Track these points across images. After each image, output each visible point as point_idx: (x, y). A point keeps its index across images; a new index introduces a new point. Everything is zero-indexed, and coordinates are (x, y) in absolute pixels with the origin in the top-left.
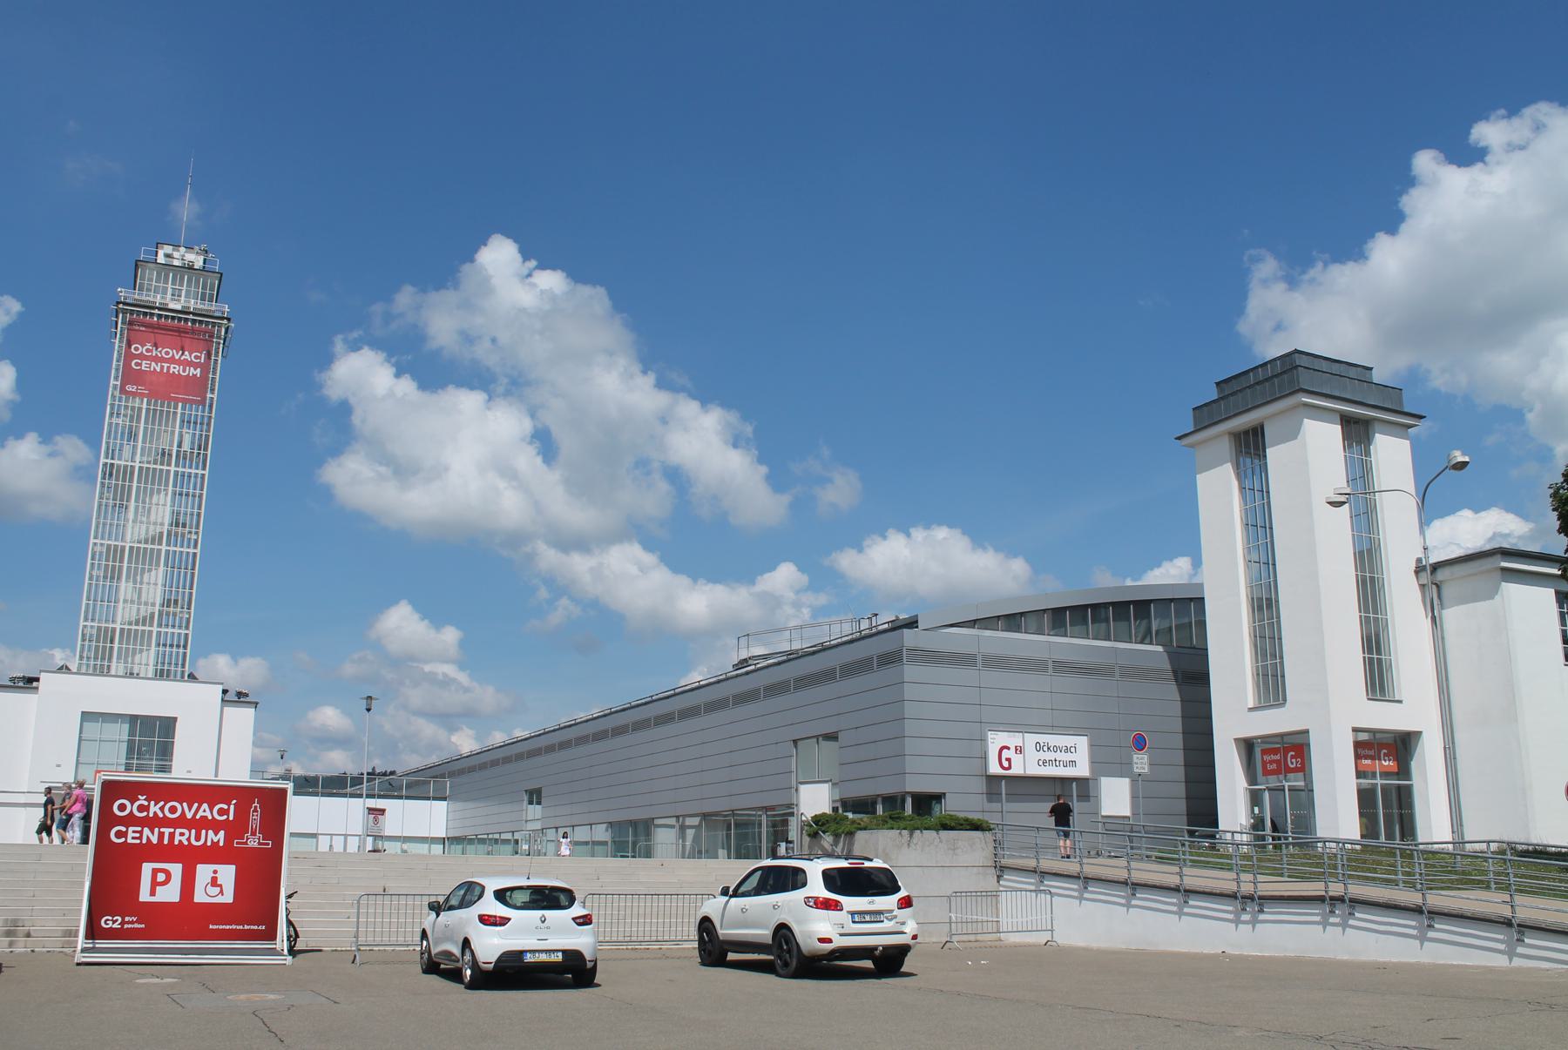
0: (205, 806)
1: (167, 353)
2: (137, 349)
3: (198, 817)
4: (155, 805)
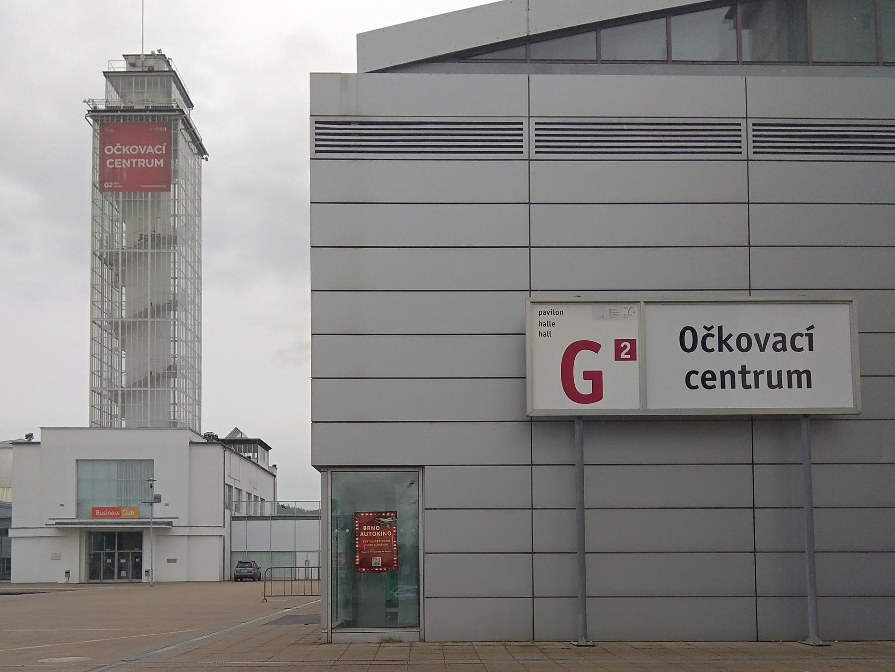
0: (150, 147)
1: (134, 150)
3: (147, 153)
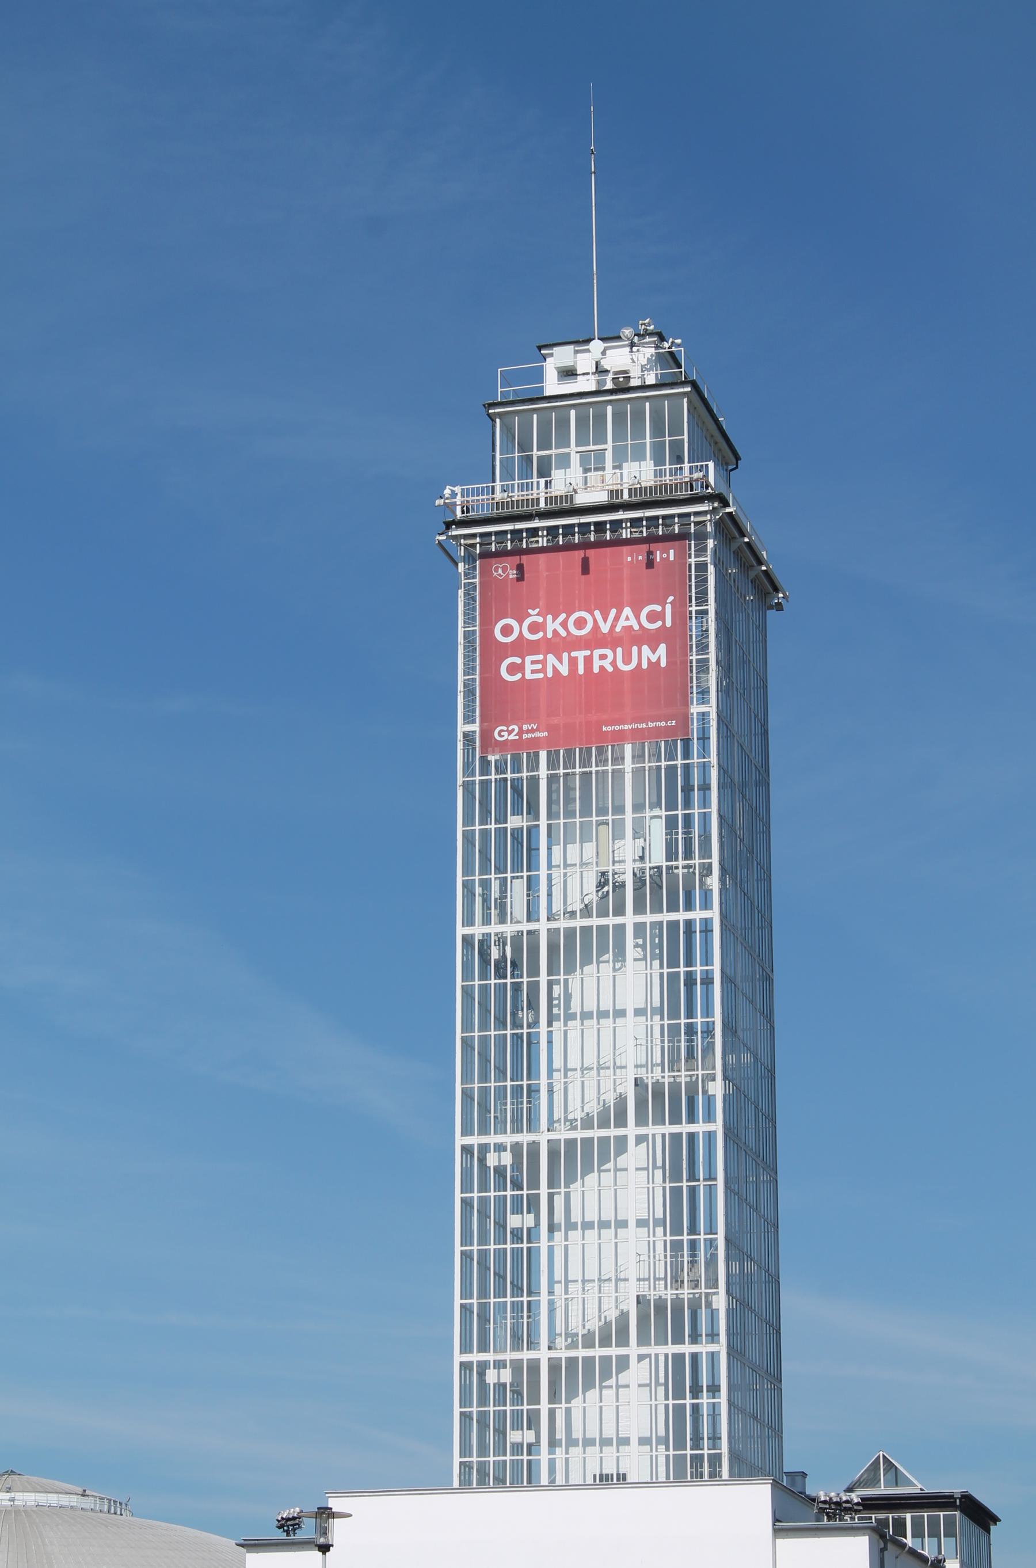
0: (627, 611)
3: (618, 629)
4: (554, 620)
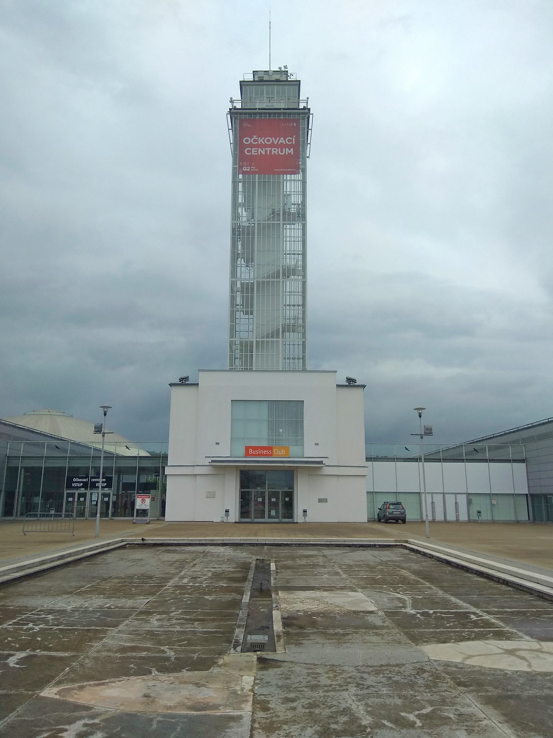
0: (282, 138)
1: (268, 141)
2: (247, 141)
3: (279, 143)
